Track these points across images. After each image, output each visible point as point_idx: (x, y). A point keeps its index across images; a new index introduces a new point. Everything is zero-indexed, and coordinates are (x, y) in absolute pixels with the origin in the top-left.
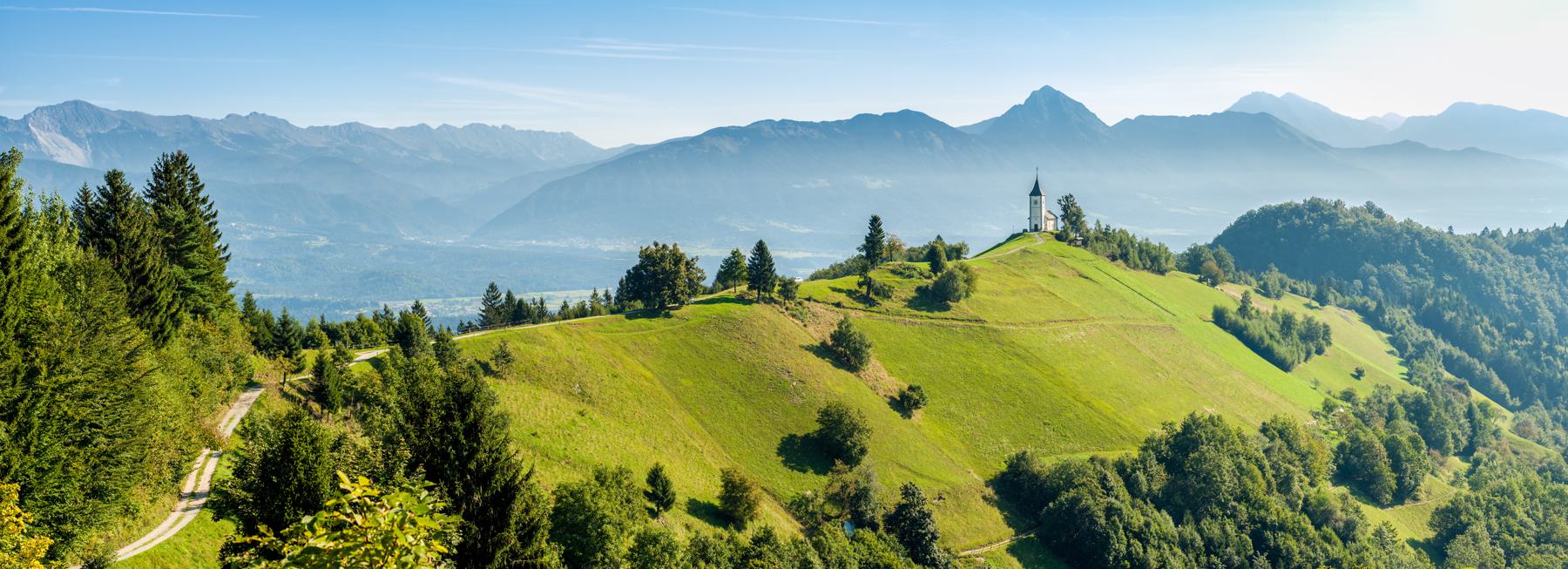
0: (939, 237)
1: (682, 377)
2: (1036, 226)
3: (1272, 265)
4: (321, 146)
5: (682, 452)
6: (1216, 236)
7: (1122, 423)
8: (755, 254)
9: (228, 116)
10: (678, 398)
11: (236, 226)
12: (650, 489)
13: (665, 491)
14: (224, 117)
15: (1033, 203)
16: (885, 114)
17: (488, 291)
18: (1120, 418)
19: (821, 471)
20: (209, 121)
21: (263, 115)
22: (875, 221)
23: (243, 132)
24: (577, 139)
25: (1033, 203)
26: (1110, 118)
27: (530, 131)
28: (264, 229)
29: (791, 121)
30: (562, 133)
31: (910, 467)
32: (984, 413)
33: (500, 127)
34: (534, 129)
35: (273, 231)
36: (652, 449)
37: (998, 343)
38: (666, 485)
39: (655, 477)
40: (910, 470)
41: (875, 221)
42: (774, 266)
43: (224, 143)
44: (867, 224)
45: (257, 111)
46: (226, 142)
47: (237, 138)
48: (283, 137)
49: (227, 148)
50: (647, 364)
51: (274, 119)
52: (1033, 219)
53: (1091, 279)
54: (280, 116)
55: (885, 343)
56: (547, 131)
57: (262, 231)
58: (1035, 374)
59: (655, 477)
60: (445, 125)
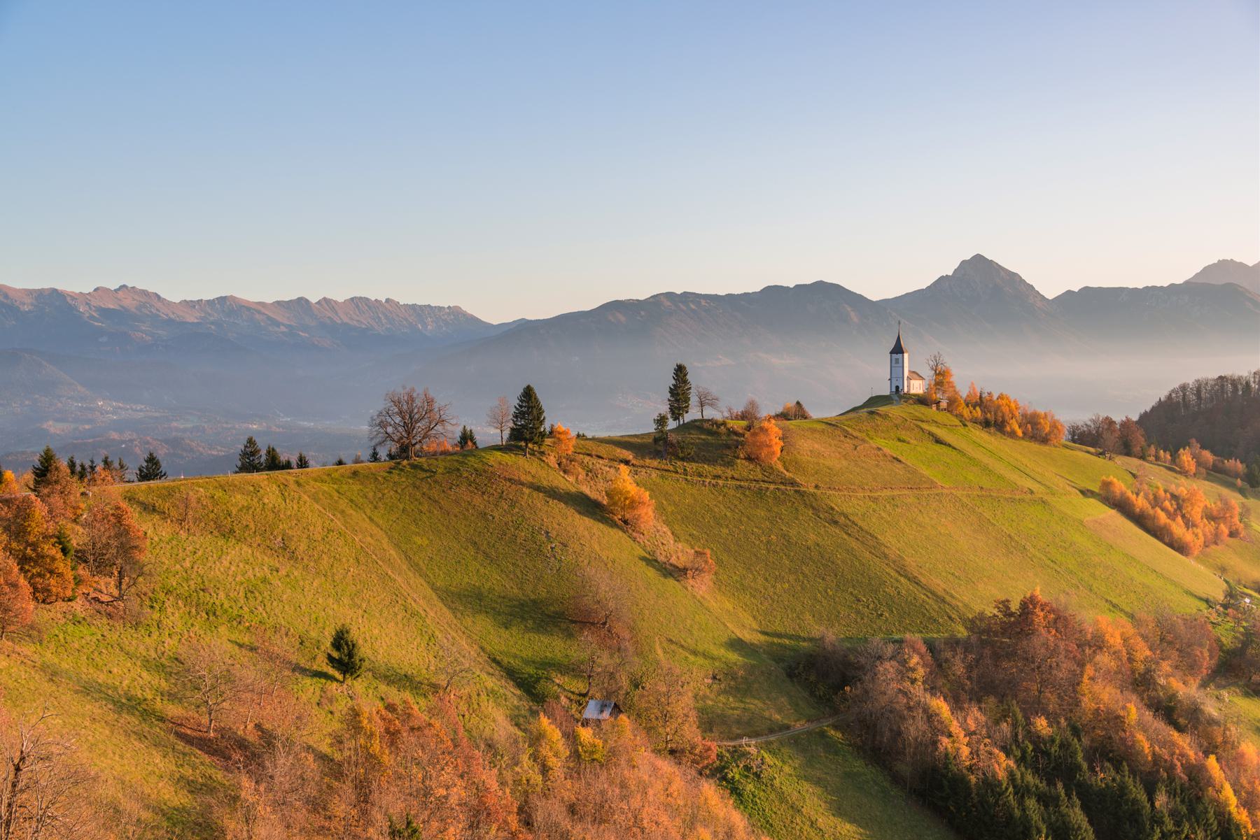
0: (798, 403)
1: (417, 534)
2: (897, 387)
3: (1194, 440)
4: (196, 321)
5: (400, 617)
6: (1143, 411)
7: (954, 602)
8: (521, 401)
9: (96, 290)
10: (408, 558)
11: (102, 406)
12: (335, 655)
13: (351, 655)
14: (91, 290)
15: (894, 362)
16: (797, 286)
17: (246, 447)
18: (952, 597)
19: (1088, 769)
20: (76, 294)
21: (133, 288)
22: (680, 371)
23: (112, 307)
24: (465, 314)
25: (894, 362)
26: (1050, 291)
27: (414, 305)
28: (132, 409)
29: (695, 293)
30: (449, 307)
31: (683, 643)
32: (786, 586)
33: (384, 301)
34: (419, 303)
35: (141, 410)
36: (361, 612)
37: (813, 508)
38: (351, 649)
39: (340, 640)
40: (682, 646)
41: (680, 371)
42: (545, 414)
43: (92, 317)
44: (671, 373)
45: (127, 284)
46: (93, 316)
47: (105, 313)
48: (154, 311)
49: (96, 324)
50: (375, 519)
51: (145, 293)
52: (894, 380)
53: (950, 445)
54: (151, 290)
55: (676, 505)
56: (433, 305)
57: (130, 411)
58: (854, 544)
59: (340, 640)
60: (325, 299)
